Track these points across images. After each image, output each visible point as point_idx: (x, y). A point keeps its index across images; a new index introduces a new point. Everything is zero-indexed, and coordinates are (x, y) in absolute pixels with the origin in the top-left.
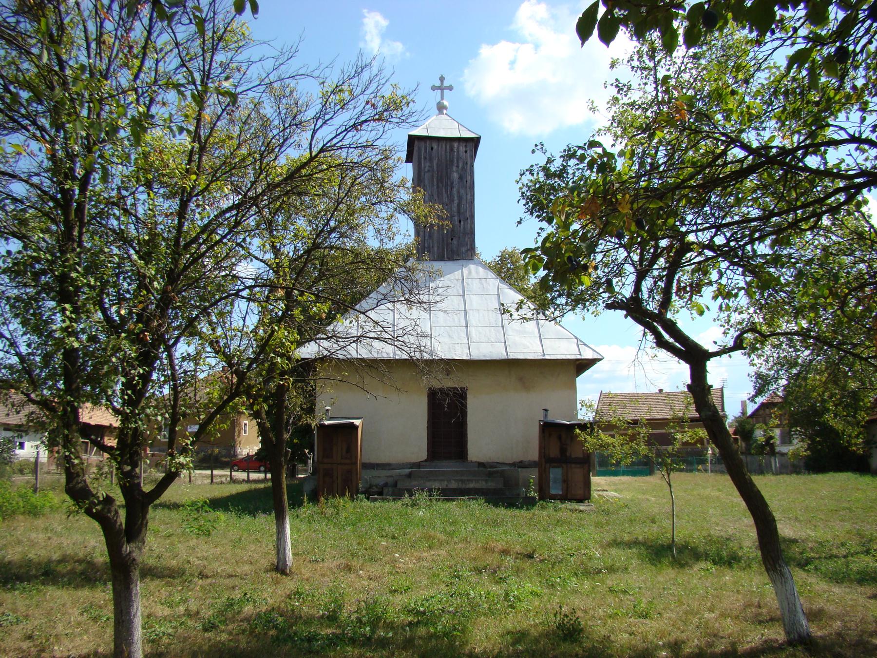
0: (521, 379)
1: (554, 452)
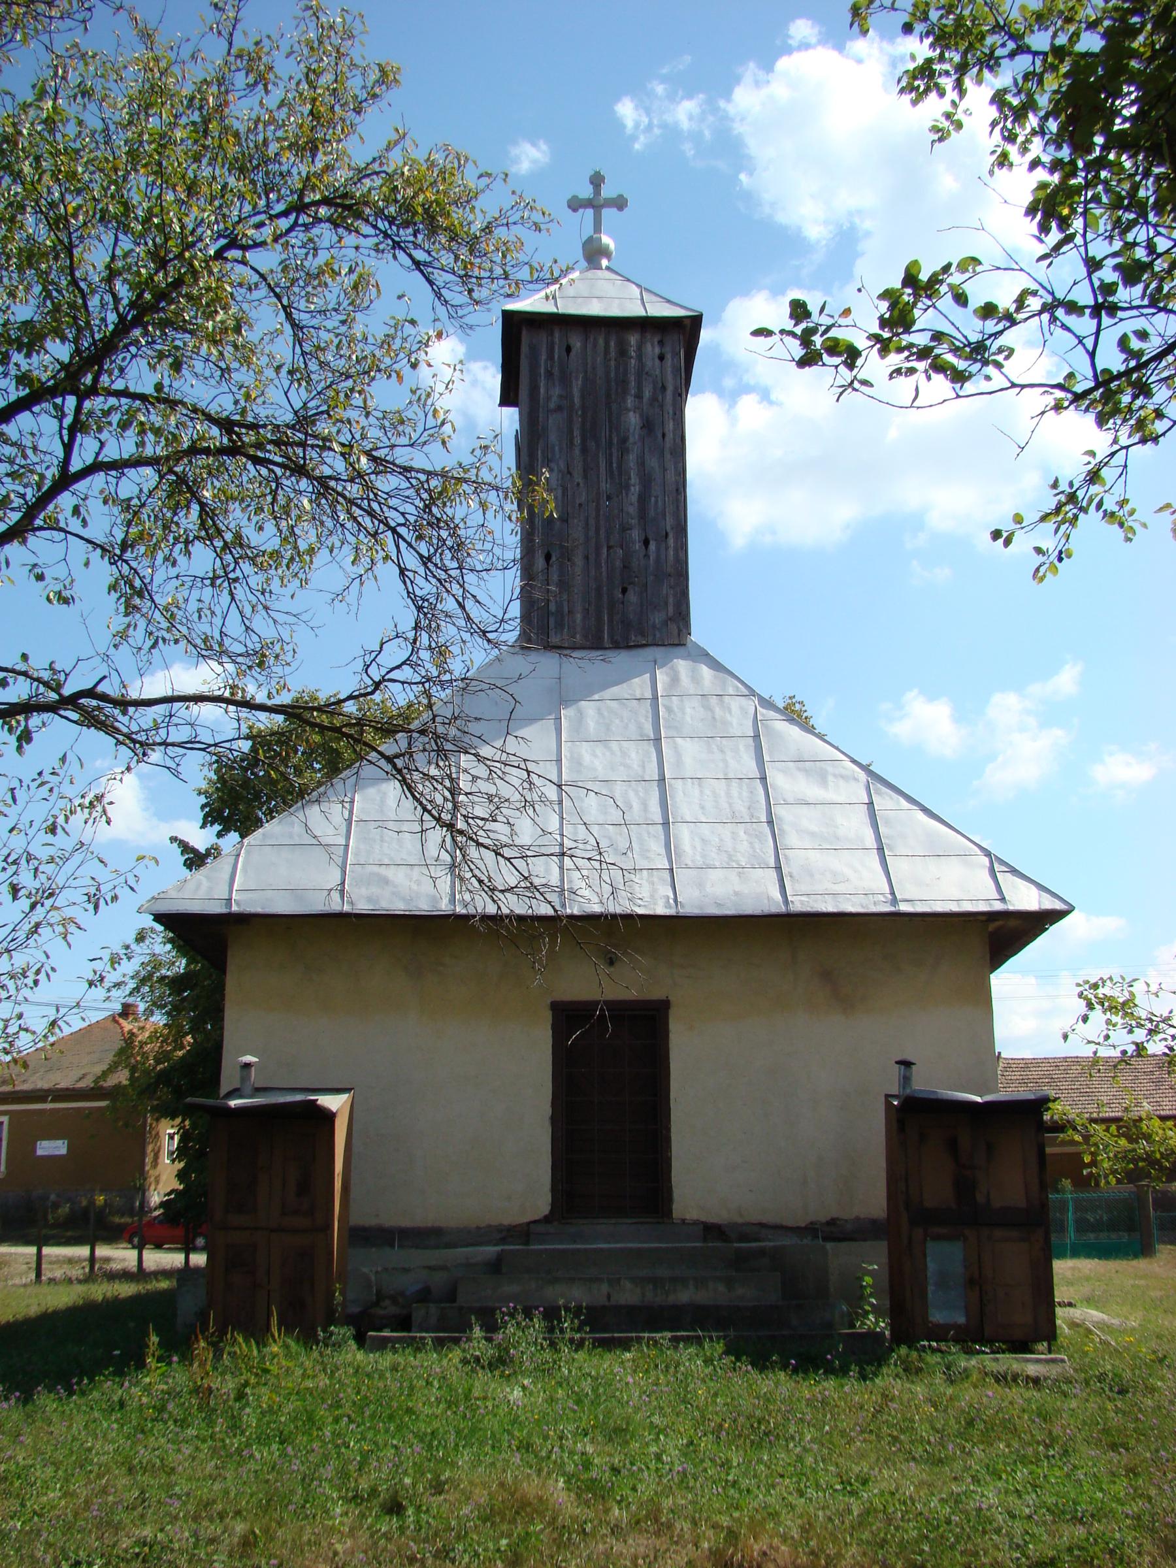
0: (827, 976)
1: (937, 1190)
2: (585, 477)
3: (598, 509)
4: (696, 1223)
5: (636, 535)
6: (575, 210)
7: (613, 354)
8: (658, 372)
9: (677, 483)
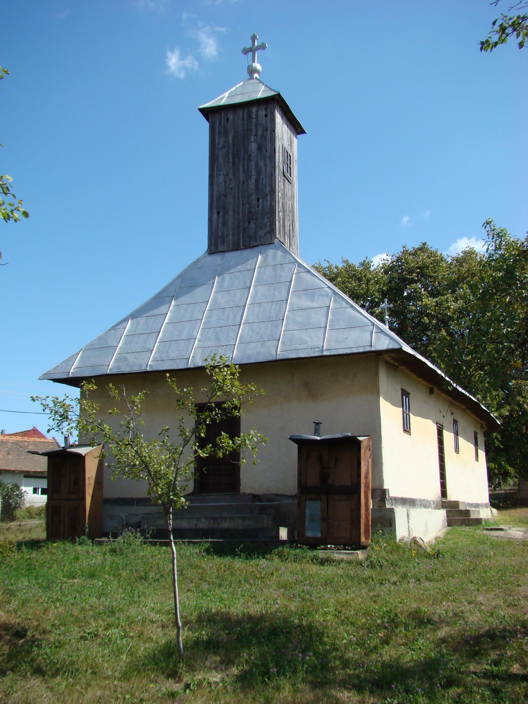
0: (306, 385)
1: (313, 479)
2: (234, 175)
3: (239, 188)
4: (249, 494)
5: (254, 197)
6: (245, 54)
7: (246, 118)
8: (264, 122)
9: (271, 171)
